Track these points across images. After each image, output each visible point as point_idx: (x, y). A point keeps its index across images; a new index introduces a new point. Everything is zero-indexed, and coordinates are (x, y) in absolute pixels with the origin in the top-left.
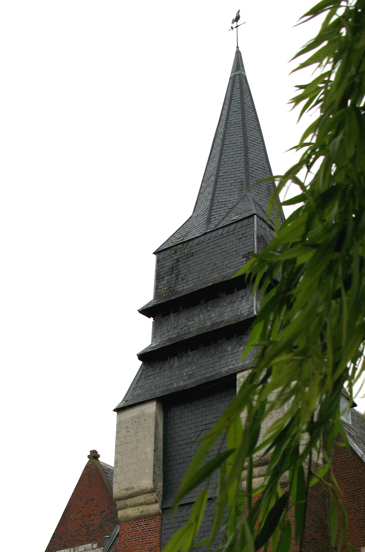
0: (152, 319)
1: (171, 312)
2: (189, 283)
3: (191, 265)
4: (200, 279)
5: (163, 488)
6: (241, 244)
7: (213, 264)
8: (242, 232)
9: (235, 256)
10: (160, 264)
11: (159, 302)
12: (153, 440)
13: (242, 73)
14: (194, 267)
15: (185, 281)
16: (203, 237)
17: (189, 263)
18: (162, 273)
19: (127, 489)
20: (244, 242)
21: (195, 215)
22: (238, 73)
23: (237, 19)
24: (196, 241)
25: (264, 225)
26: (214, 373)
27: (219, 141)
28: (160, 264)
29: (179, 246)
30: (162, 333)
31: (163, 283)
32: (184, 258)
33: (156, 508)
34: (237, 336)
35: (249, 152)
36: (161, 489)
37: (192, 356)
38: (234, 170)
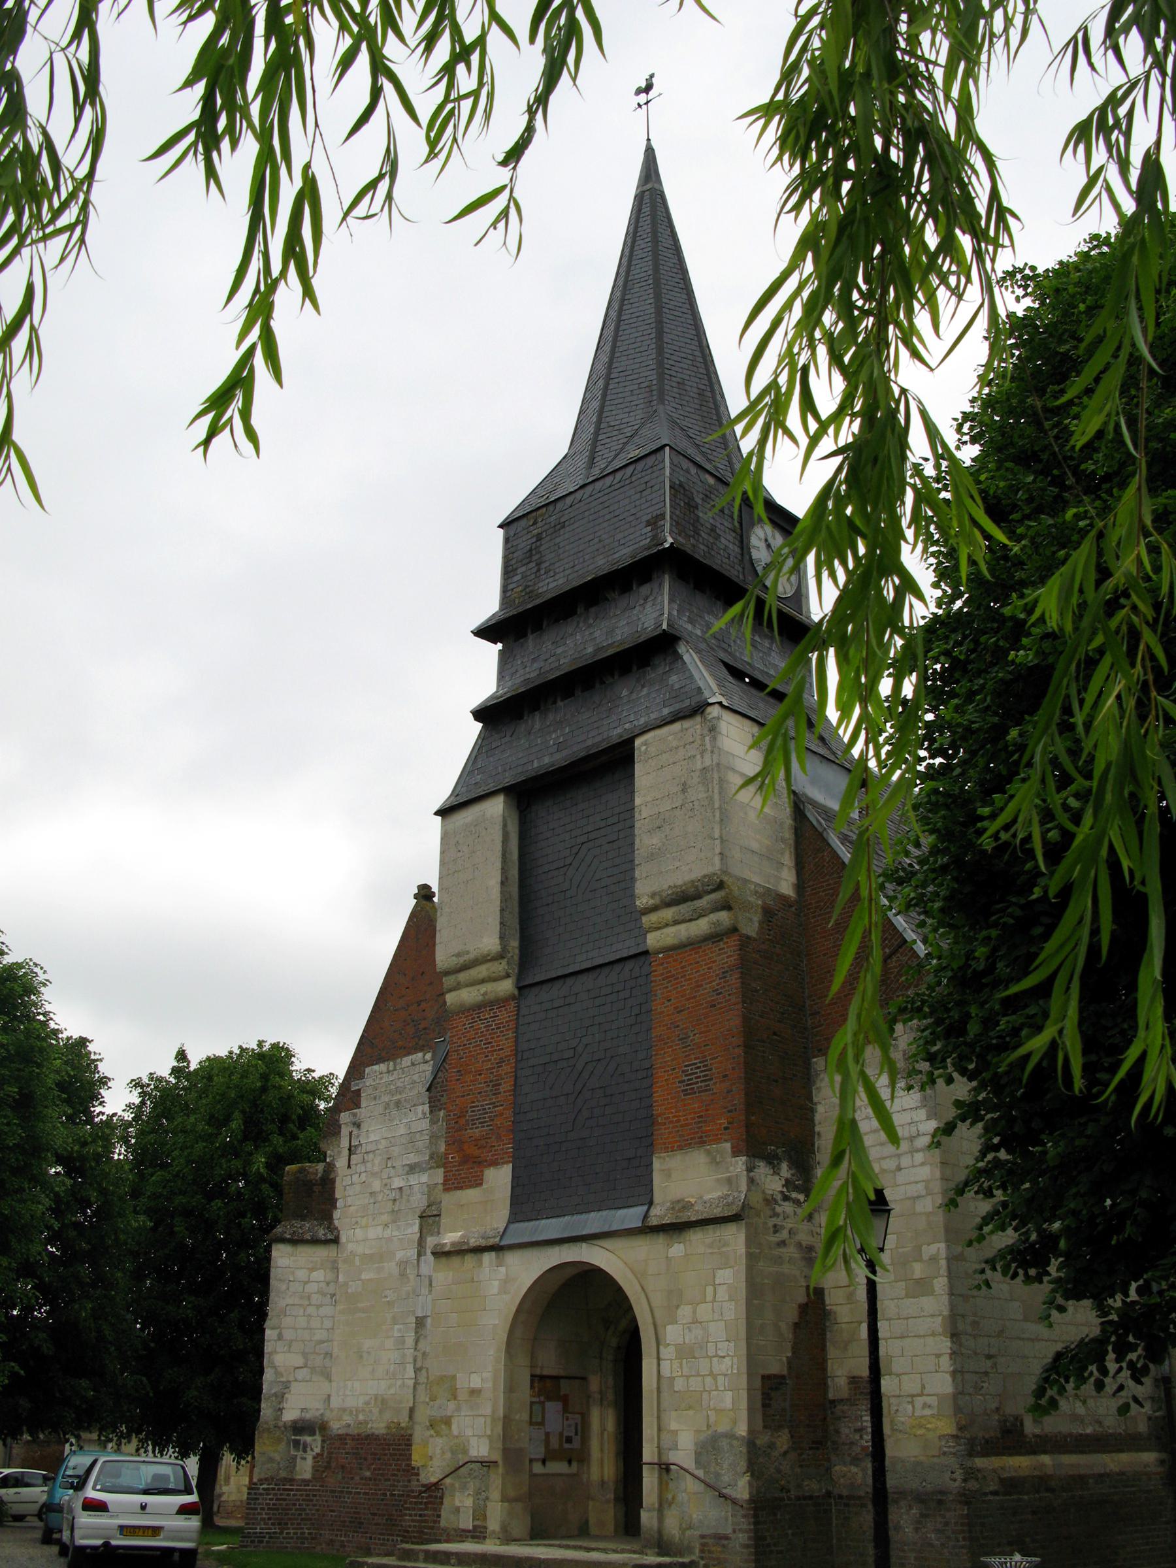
0: (500, 646)
1: (529, 631)
2: (557, 577)
3: (561, 545)
4: (576, 568)
5: (521, 951)
6: (643, 500)
7: (596, 540)
8: (646, 479)
9: (633, 523)
10: (509, 545)
11: (511, 614)
12: (499, 865)
13: (656, 186)
14: (567, 548)
15: (552, 573)
16: (581, 492)
17: (558, 540)
18: (514, 562)
19: (458, 955)
20: (649, 498)
21: (572, 452)
22: (649, 186)
23: (648, 88)
24: (569, 500)
25: (685, 464)
26: (598, 739)
27: (613, 314)
28: (509, 545)
29: (540, 512)
30: (513, 670)
31: (516, 578)
32: (549, 532)
33: (507, 986)
34: (639, 668)
35: (666, 330)
36: (517, 951)
37: (563, 709)
38: (637, 366)
